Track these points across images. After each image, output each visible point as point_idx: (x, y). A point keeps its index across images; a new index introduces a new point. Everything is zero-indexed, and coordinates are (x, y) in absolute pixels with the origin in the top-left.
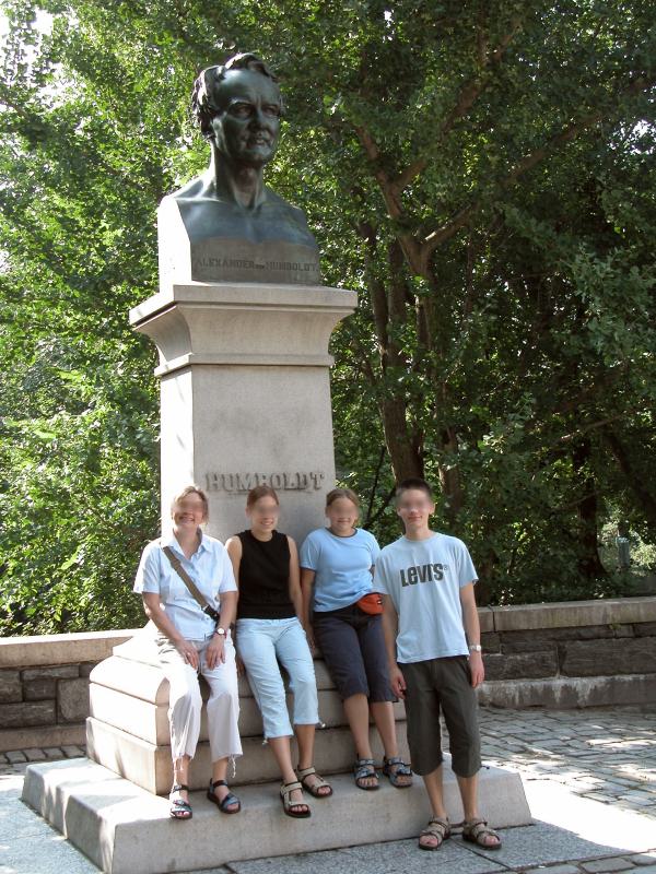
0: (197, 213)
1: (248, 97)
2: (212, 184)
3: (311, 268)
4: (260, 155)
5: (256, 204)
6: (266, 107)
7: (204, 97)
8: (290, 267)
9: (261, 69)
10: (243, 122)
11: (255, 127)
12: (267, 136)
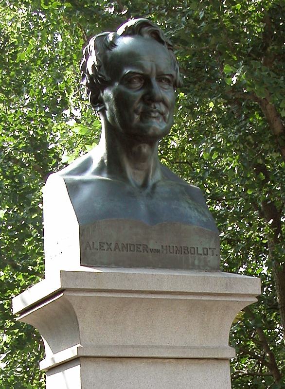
0: (86, 192)
1: (141, 67)
2: (102, 161)
3: (210, 252)
4: (155, 129)
5: (151, 182)
6: (161, 78)
7: (93, 66)
8: (188, 251)
9: (156, 36)
10: (136, 93)
11: (149, 99)
12: (163, 108)
